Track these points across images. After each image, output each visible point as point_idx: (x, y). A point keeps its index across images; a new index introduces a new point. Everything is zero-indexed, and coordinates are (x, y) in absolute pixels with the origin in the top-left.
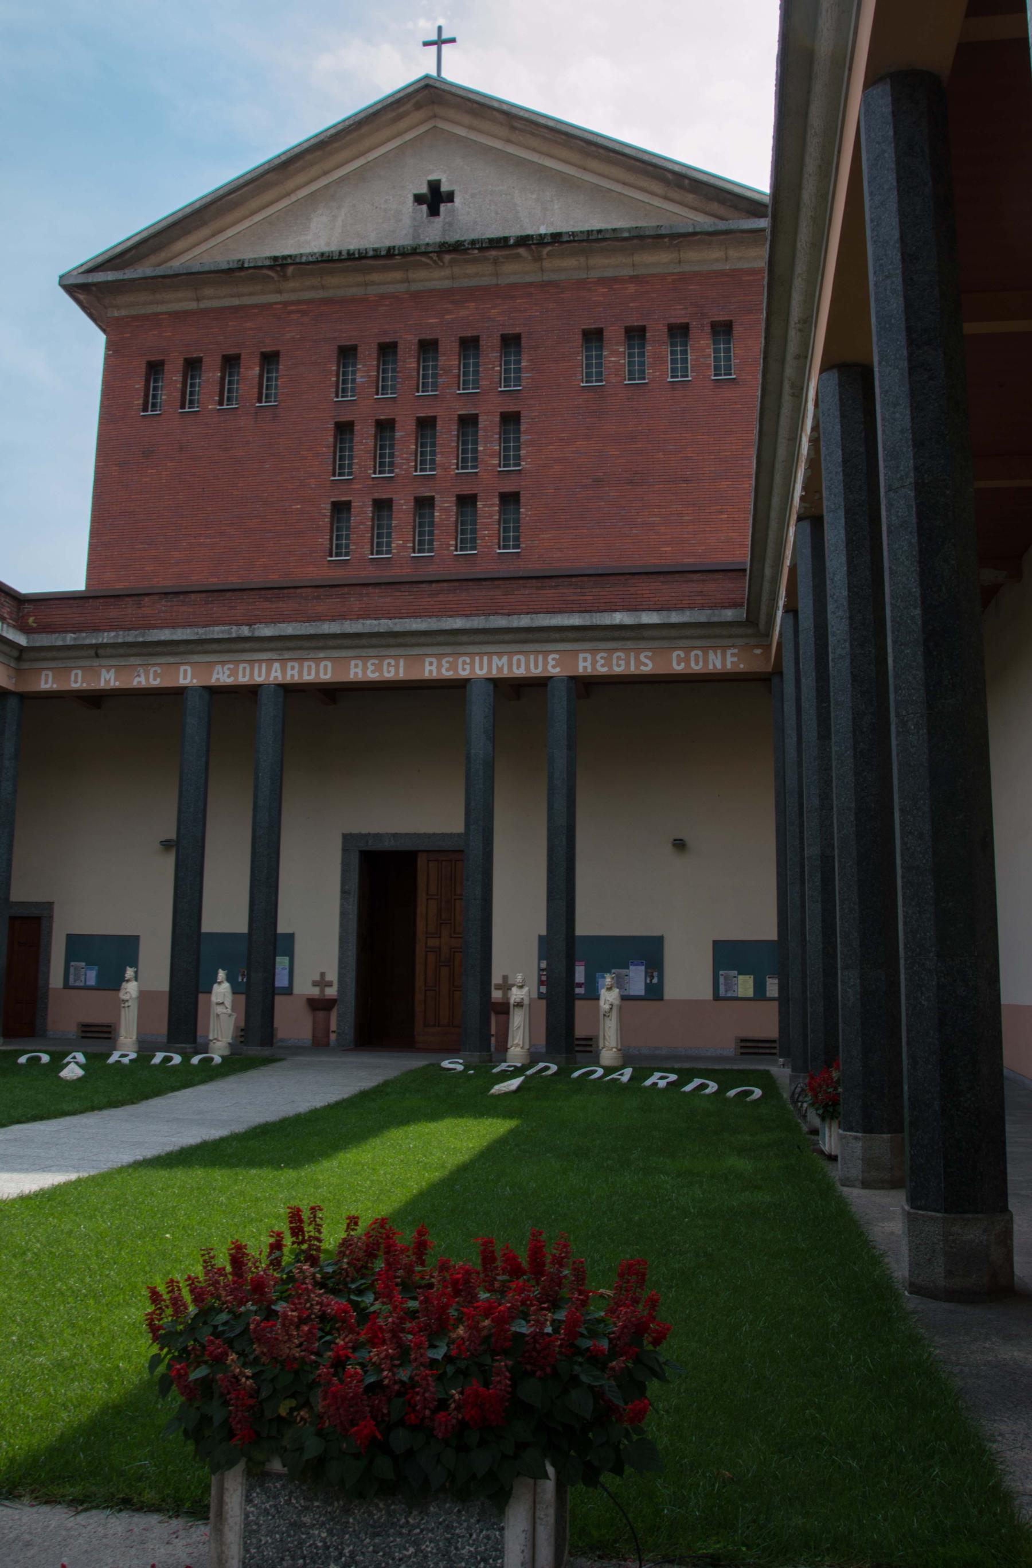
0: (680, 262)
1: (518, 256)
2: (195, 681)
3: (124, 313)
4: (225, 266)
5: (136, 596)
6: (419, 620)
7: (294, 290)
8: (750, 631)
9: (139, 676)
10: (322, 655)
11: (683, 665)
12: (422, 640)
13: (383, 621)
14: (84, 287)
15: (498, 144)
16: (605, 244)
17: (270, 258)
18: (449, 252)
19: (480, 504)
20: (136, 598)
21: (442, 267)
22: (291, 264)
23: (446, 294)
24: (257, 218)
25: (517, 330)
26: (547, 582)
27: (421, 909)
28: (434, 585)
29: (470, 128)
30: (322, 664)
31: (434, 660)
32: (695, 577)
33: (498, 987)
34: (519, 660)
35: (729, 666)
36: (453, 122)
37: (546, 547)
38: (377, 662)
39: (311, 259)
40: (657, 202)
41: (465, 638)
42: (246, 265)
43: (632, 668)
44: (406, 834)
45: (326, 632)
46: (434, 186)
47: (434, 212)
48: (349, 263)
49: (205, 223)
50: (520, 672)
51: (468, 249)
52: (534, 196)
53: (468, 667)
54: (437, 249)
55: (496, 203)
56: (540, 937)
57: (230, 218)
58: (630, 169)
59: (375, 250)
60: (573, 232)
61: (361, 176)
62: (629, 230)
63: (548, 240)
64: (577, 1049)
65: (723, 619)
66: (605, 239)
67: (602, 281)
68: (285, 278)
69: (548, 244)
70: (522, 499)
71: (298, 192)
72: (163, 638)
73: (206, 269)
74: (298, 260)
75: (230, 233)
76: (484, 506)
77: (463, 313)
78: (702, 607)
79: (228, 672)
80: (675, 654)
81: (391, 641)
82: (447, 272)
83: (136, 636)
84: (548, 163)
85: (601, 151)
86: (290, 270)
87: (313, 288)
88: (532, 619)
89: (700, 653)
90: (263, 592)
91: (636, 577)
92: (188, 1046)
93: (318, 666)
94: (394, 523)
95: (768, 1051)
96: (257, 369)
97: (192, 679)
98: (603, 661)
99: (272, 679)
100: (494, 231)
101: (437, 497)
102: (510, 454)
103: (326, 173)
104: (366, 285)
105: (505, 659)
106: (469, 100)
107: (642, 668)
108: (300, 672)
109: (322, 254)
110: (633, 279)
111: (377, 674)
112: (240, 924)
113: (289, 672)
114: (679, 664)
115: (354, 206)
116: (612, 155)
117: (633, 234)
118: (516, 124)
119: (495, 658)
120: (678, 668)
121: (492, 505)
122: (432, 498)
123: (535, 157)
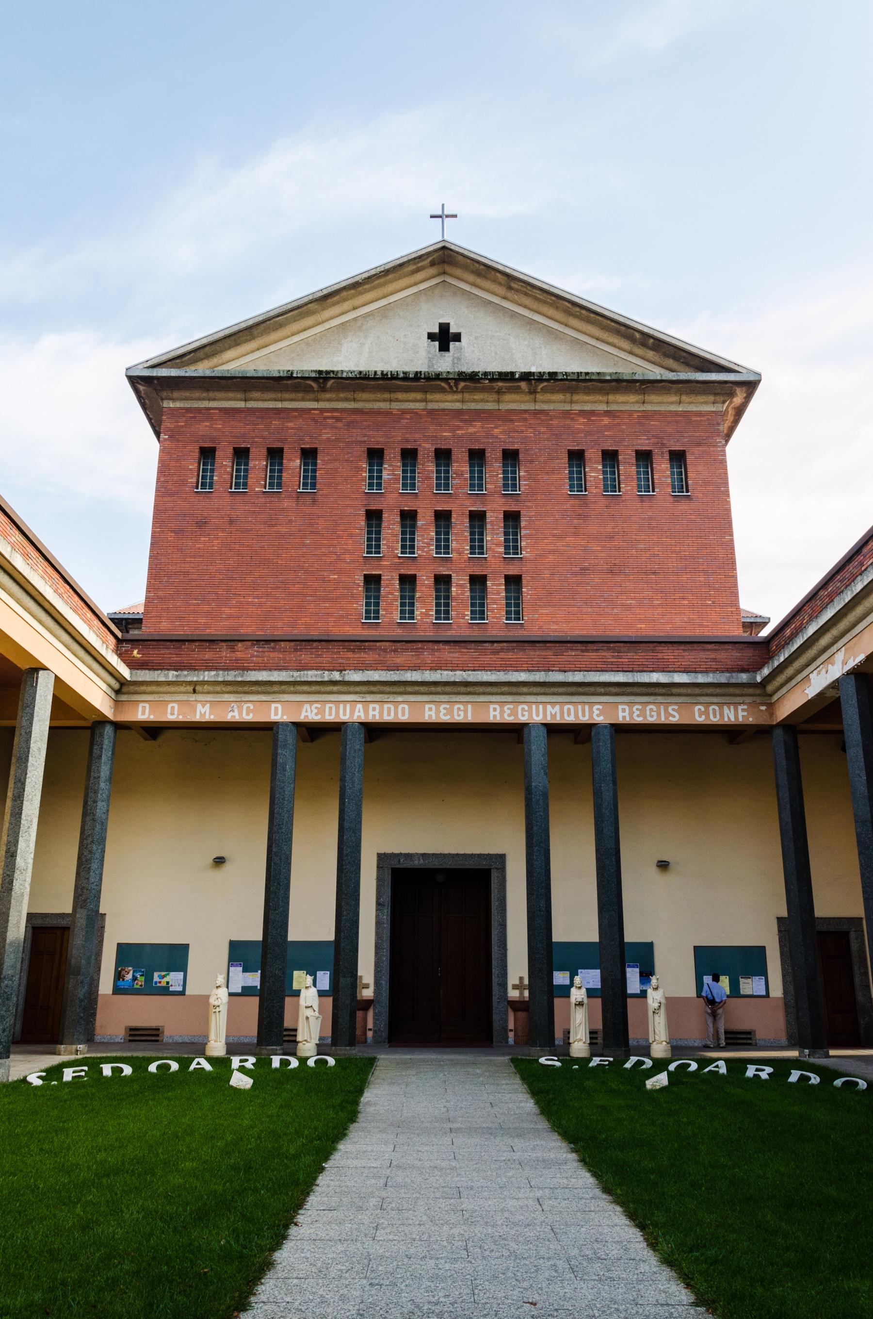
1: (519, 387)
2: (285, 717)
3: (178, 404)
4: (276, 374)
5: (231, 642)
6: (489, 673)
7: (329, 400)
8: (758, 691)
9: (233, 711)
10: (400, 698)
11: (703, 717)
12: (489, 689)
13: (458, 673)
14: (147, 380)
15: (496, 300)
17: (315, 371)
18: (464, 380)
19: (489, 583)
20: (229, 643)
21: (455, 392)
23: (458, 413)
25: (516, 447)
26: (590, 646)
28: (495, 645)
31: (497, 706)
32: (709, 646)
33: (515, 987)
34: (569, 709)
37: (542, 619)
38: (448, 706)
39: (350, 375)
41: (525, 690)
42: (295, 375)
43: (663, 719)
44: (433, 854)
45: (409, 679)
46: (444, 328)
47: (444, 348)
49: (253, 338)
50: (570, 719)
51: (482, 379)
52: (526, 343)
53: (526, 713)
54: (456, 377)
55: (494, 344)
57: (274, 336)
59: (404, 373)
61: (383, 313)
62: (611, 374)
63: (546, 377)
64: (285, 1033)
65: (739, 681)
66: (591, 380)
67: (583, 413)
68: (323, 389)
69: (546, 380)
70: (524, 582)
71: (331, 322)
72: (260, 679)
73: (260, 375)
74: (339, 375)
75: (273, 348)
76: (493, 585)
77: (472, 430)
78: (715, 671)
79: (315, 711)
80: (697, 708)
81: (463, 689)
82: (458, 396)
83: (235, 676)
85: (584, 312)
86: (330, 383)
87: (346, 400)
88: (584, 676)
89: (716, 708)
90: (347, 644)
91: (663, 645)
92: (278, 1048)
93: (396, 708)
94: (418, 595)
95: (745, 1041)
96: (298, 461)
97: (150, 714)
98: (638, 712)
100: (495, 367)
102: (512, 545)
103: (354, 308)
104: (391, 401)
105: (557, 707)
106: (478, 262)
107: (671, 718)
108: (381, 713)
109: (360, 372)
110: (607, 413)
111: (449, 717)
112: (592, 935)
113: (371, 713)
114: (700, 717)
115: (378, 337)
116: (592, 315)
117: (614, 377)
118: (513, 285)
119: (549, 707)
120: (700, 719)
121: (500, 584)
122: (450, 576)
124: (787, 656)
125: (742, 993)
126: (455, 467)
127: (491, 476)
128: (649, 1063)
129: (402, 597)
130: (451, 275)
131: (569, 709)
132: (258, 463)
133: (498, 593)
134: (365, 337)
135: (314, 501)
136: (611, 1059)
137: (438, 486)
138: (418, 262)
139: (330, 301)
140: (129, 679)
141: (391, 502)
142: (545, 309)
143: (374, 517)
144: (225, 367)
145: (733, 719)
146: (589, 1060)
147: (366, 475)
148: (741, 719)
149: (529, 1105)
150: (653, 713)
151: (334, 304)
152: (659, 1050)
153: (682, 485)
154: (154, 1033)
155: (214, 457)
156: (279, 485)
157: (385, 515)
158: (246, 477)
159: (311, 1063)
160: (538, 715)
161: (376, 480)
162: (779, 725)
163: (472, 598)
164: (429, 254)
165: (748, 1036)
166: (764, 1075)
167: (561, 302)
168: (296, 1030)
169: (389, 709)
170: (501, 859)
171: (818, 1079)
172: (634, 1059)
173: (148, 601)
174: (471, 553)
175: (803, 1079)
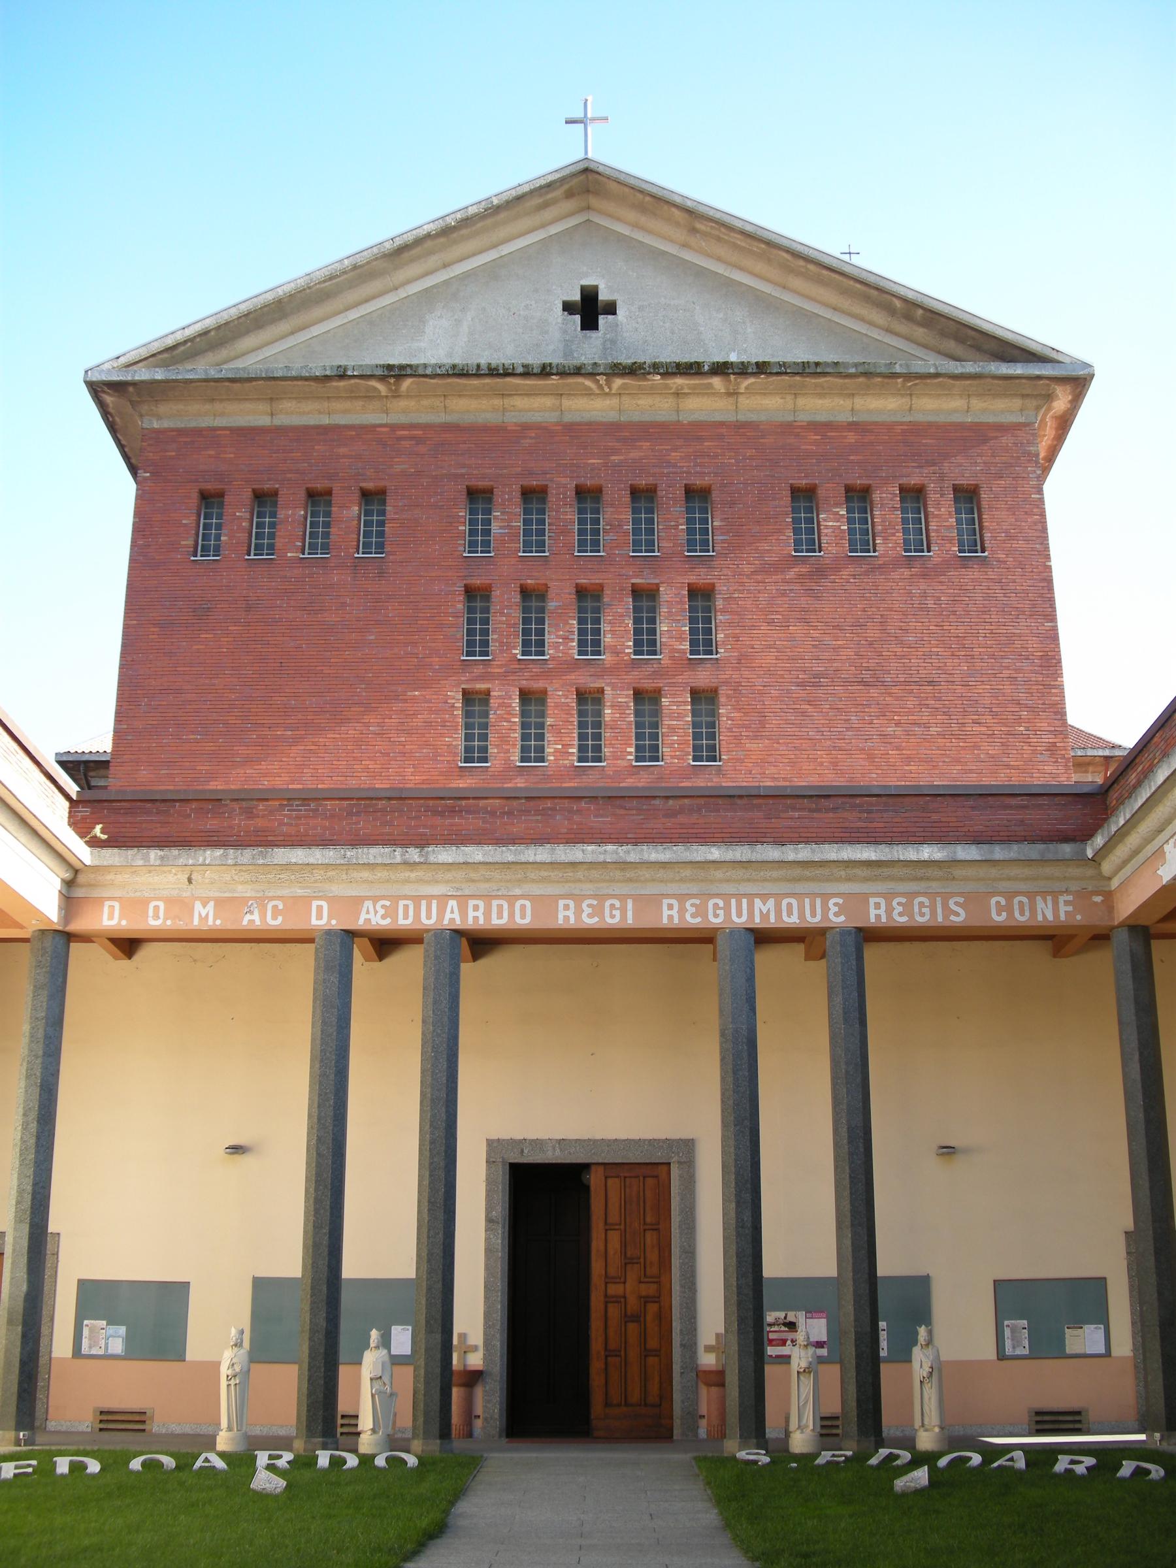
0: (910, 409)
1: (710, 386)
8: (1090, 872)
9: (251, 912)
11: (1004, 914)
14: (117, 387)
16: (822, 380)
17: (383, 366)
22: (411, 376)
24: (353, 315)
27: (596, 1244)
29: (636, 226)
30: (518, 903)
34: (790, 905)
35: (1063, 917)
36: (610, 216)
37: (747, 763)
40: (875, 334)
42: (349, 373)
47: (590, 324)
48: (487, 381)
52: (721, 315)
53: (721, 912)
55: (658, 317)
56: (262, 1287)
58: (845, 292)
60: (784, 363)
61: (492, 272)
62: (856, 365)
69: (753, 374)
74: (421, 372)
75: (316, 330)
77: (635, 454)
79: (381, 912)
80: (993, 901)
84: (738, 276)
85: (811, 267)
89: (794, 902)
94: (549, 721)
97: (121, 919)
98: (901, 909)
99: (446, 922)
101: (608, 690)
102: (702, 641)
103: (445, 266)
105: (771, 903)
106: (641, 192)
107: (953, 918)
108: (487, 914)
109: (454, 367)
111: (596, 919)
113: (471, 914)
114: (999, 914)
115: (484, 309)
116: (825, 272)
117: (861, 369)
118: (698, 226)
119: (758, 902)
121: (685, 703)
123: (720, 269)
124: (1128, 816)
125: (1068, 1351)
126: (607, 515)
127: (669, 528)
128: (906, 1456)
129: (524, 726)
130: (600, 212)
131: (790, 905)
132: (292, 513)
133: (680, 717)
134: (463, 310)
135: (381, 574)
136: (849, 1453)
137: (582, 544)
138: (547, 193)
139: (406, 255)
140: (88, 862)
141: (505, 578)
142: (748, 263)
143: (476, 596)
144: (239, 364)
145: (1050, 917)
146: (818, 1455)
147: (464, 528)
148: (1063, 917)
149: (710, 1516)
150: (924, 910)
151: (412, 260)
152: (926, 1441)
153: (973, 541)
154: (137, 1418)
155: (221, 505)
156: (326, 548)
157: (496, 593)
158: (272, 536)
159: (380, 1461)
160: (739, 915)
161: (480, 537)
162: (1121, 925)
163: (638, 725)
164: (563, 180)
165: (1077, 1418)
166: (1080, 1469)
167: (775, 252)
168: (357, 1417)
169: (500, 907)
170: (687, 1146)
171: (1162, 1472)
172: (883, 1452)
173: (118, 735)
174: (635, 653)
175: (1140, 1473)
